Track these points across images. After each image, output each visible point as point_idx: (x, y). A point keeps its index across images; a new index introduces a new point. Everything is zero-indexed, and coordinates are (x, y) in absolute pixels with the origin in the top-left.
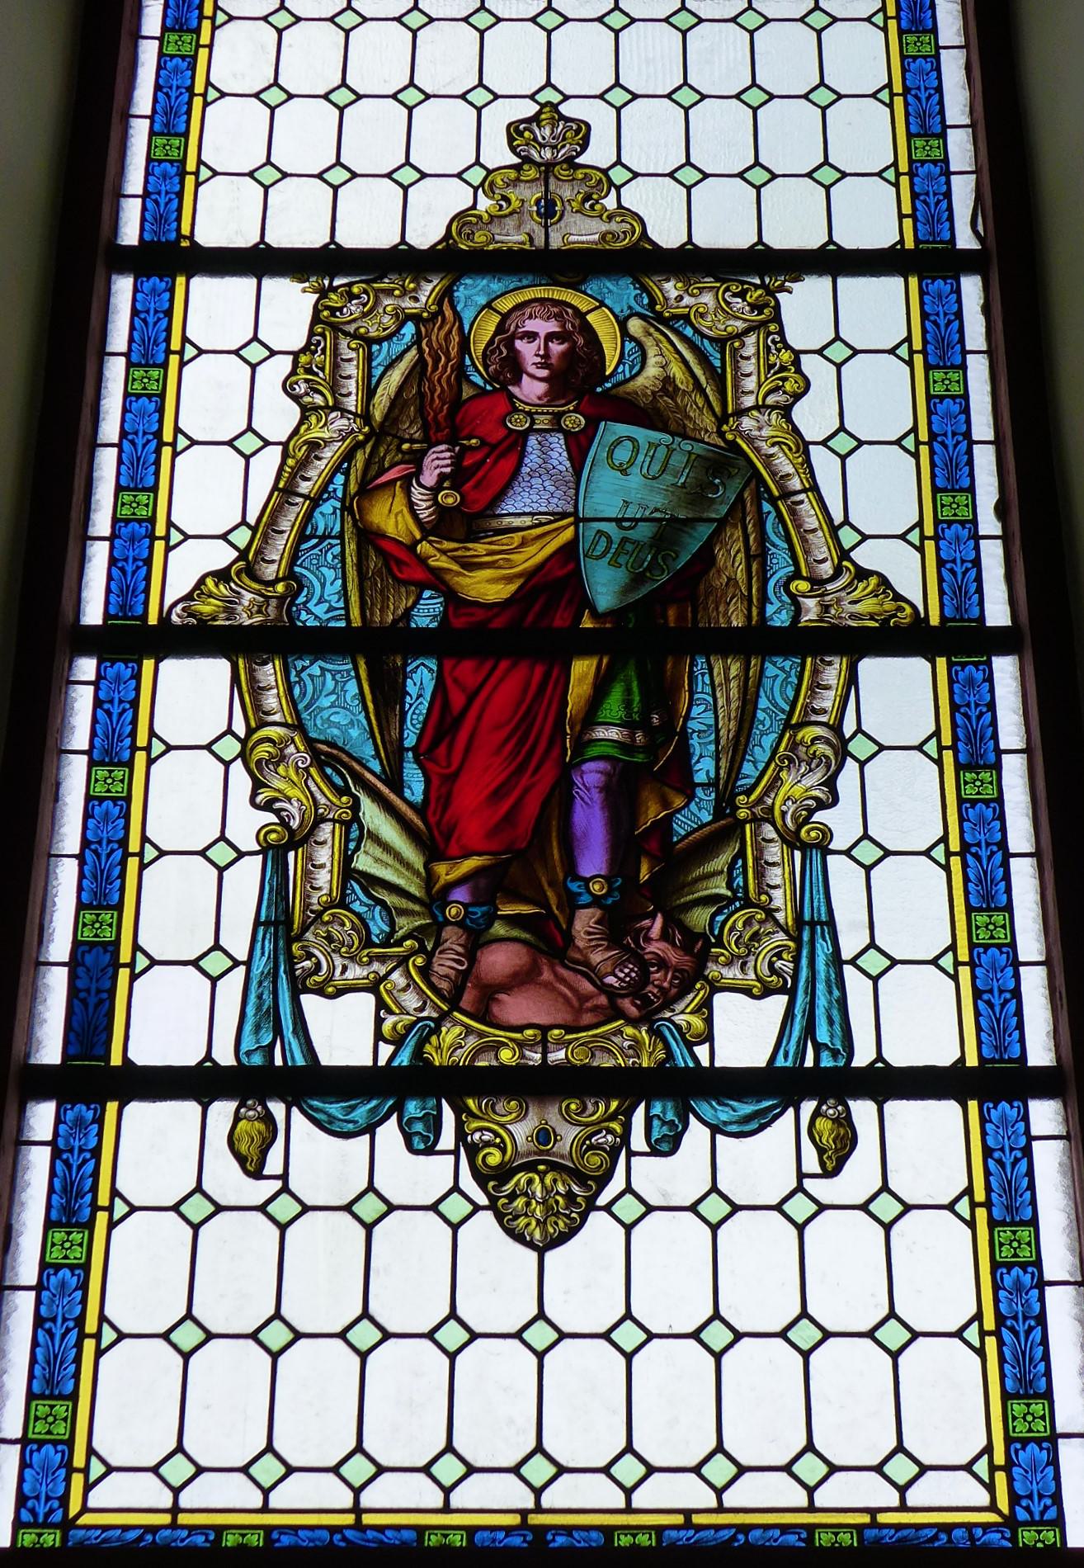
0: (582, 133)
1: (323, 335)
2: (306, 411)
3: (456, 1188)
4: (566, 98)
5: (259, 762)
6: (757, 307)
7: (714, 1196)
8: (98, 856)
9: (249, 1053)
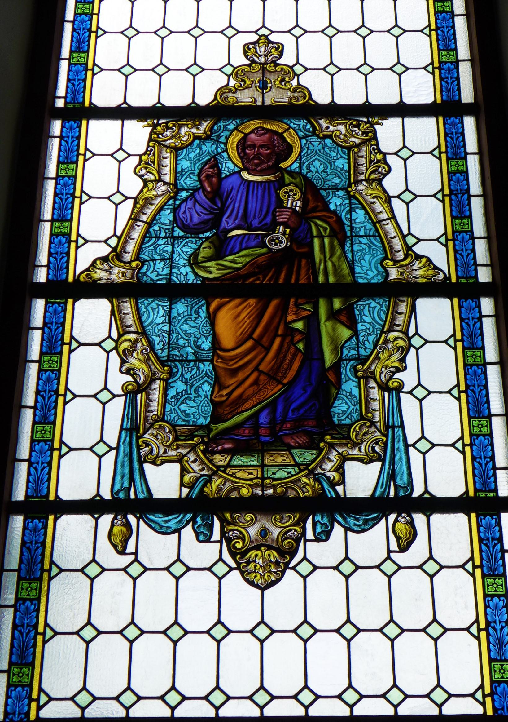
0: (280, 49)
1: (154, 147)
2: (146, 183)
3: (220, 559)
4: (272, 32)
5: (124, 351)
6: (365, 133)
7: (348, 624)
8: (51, 330)
9: (119, 491)
